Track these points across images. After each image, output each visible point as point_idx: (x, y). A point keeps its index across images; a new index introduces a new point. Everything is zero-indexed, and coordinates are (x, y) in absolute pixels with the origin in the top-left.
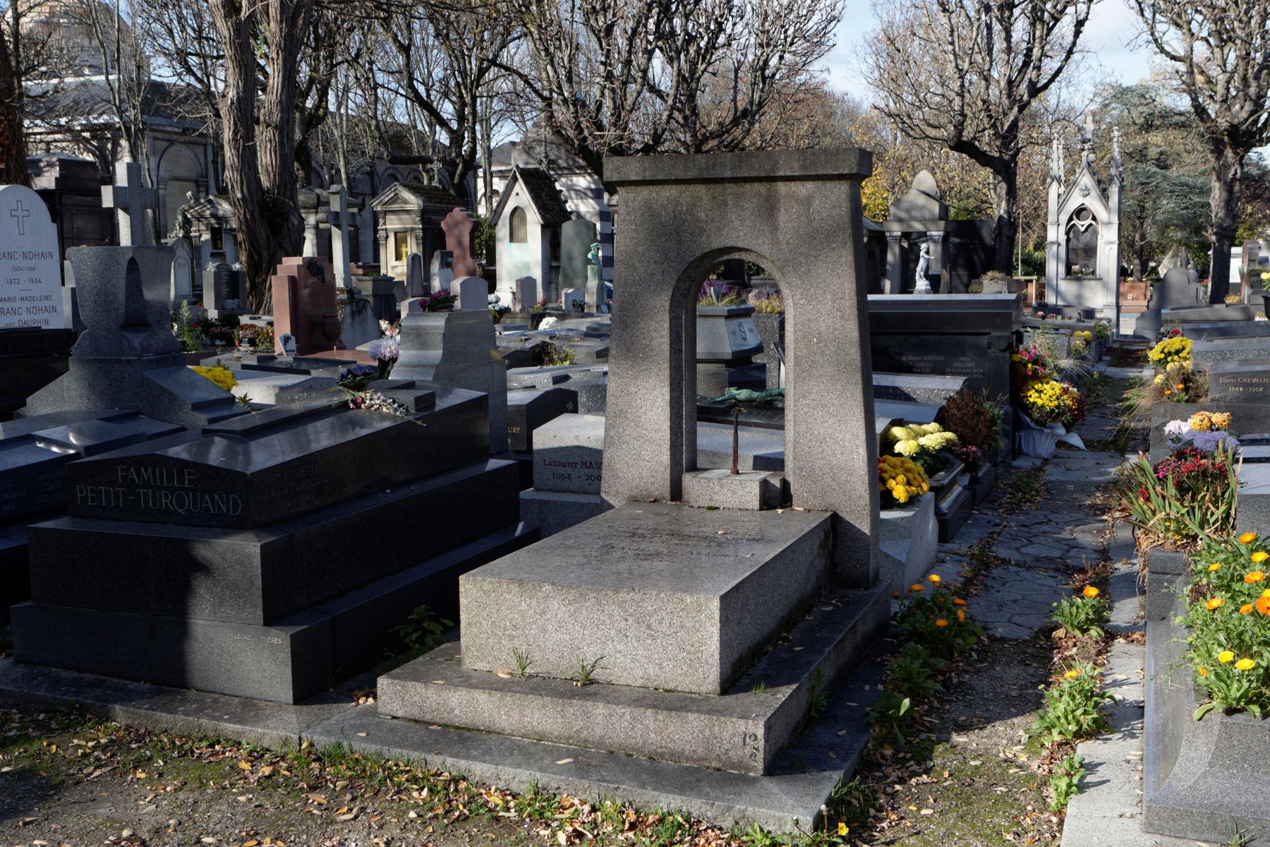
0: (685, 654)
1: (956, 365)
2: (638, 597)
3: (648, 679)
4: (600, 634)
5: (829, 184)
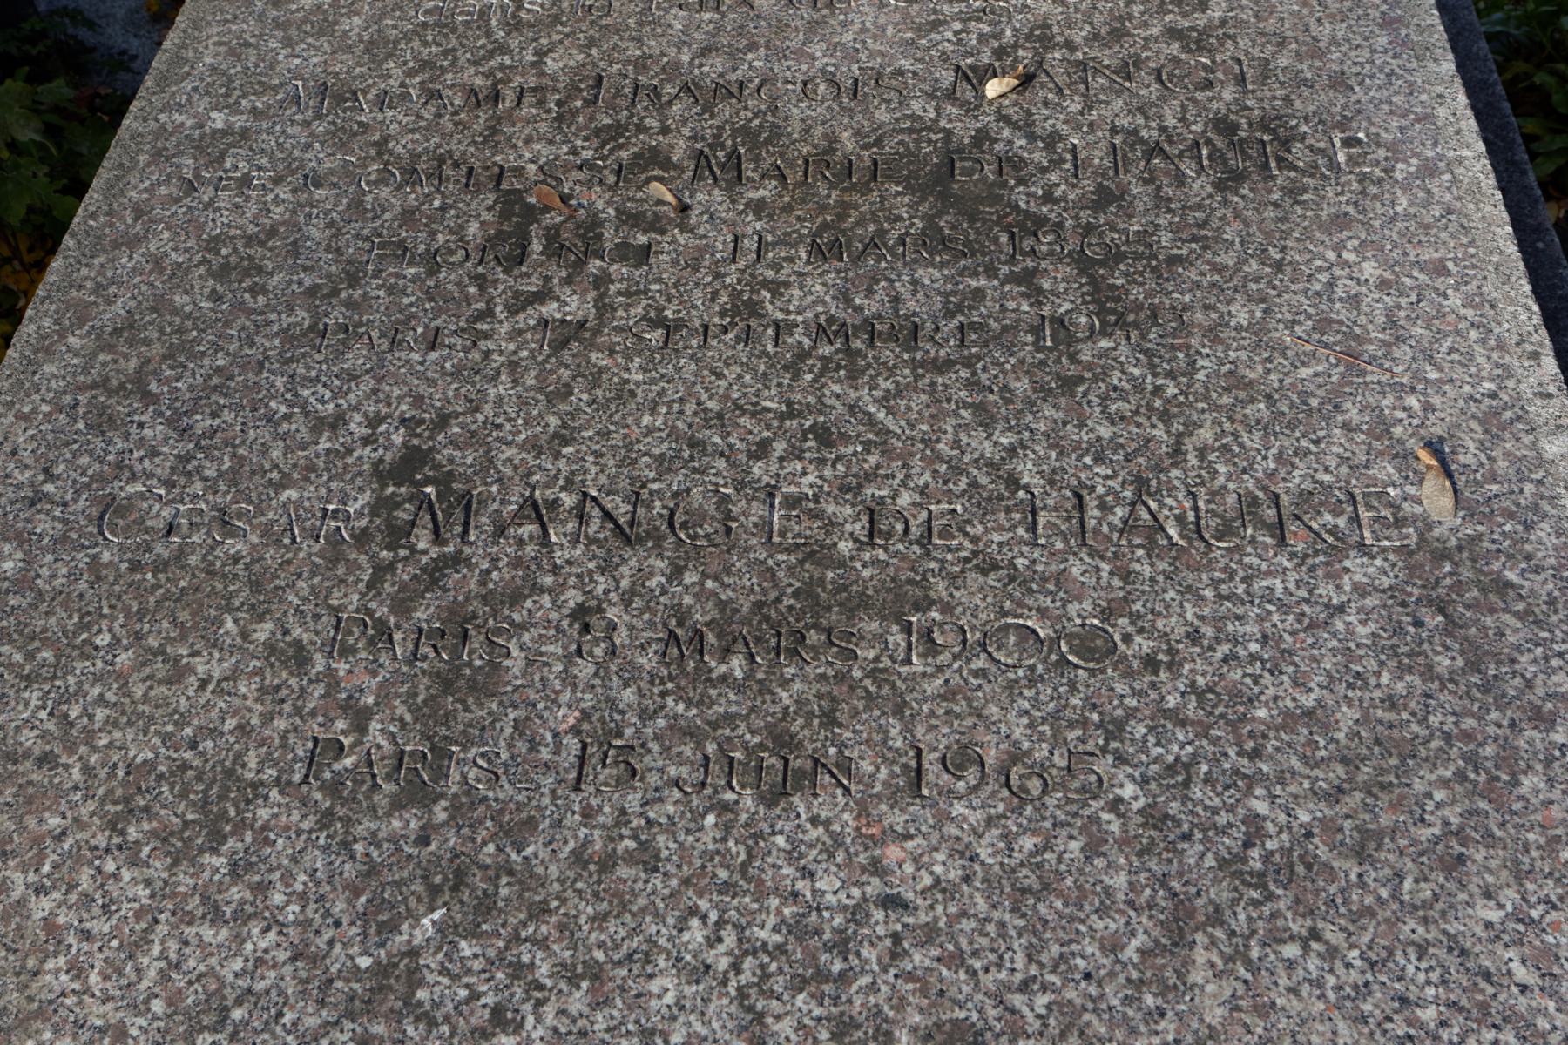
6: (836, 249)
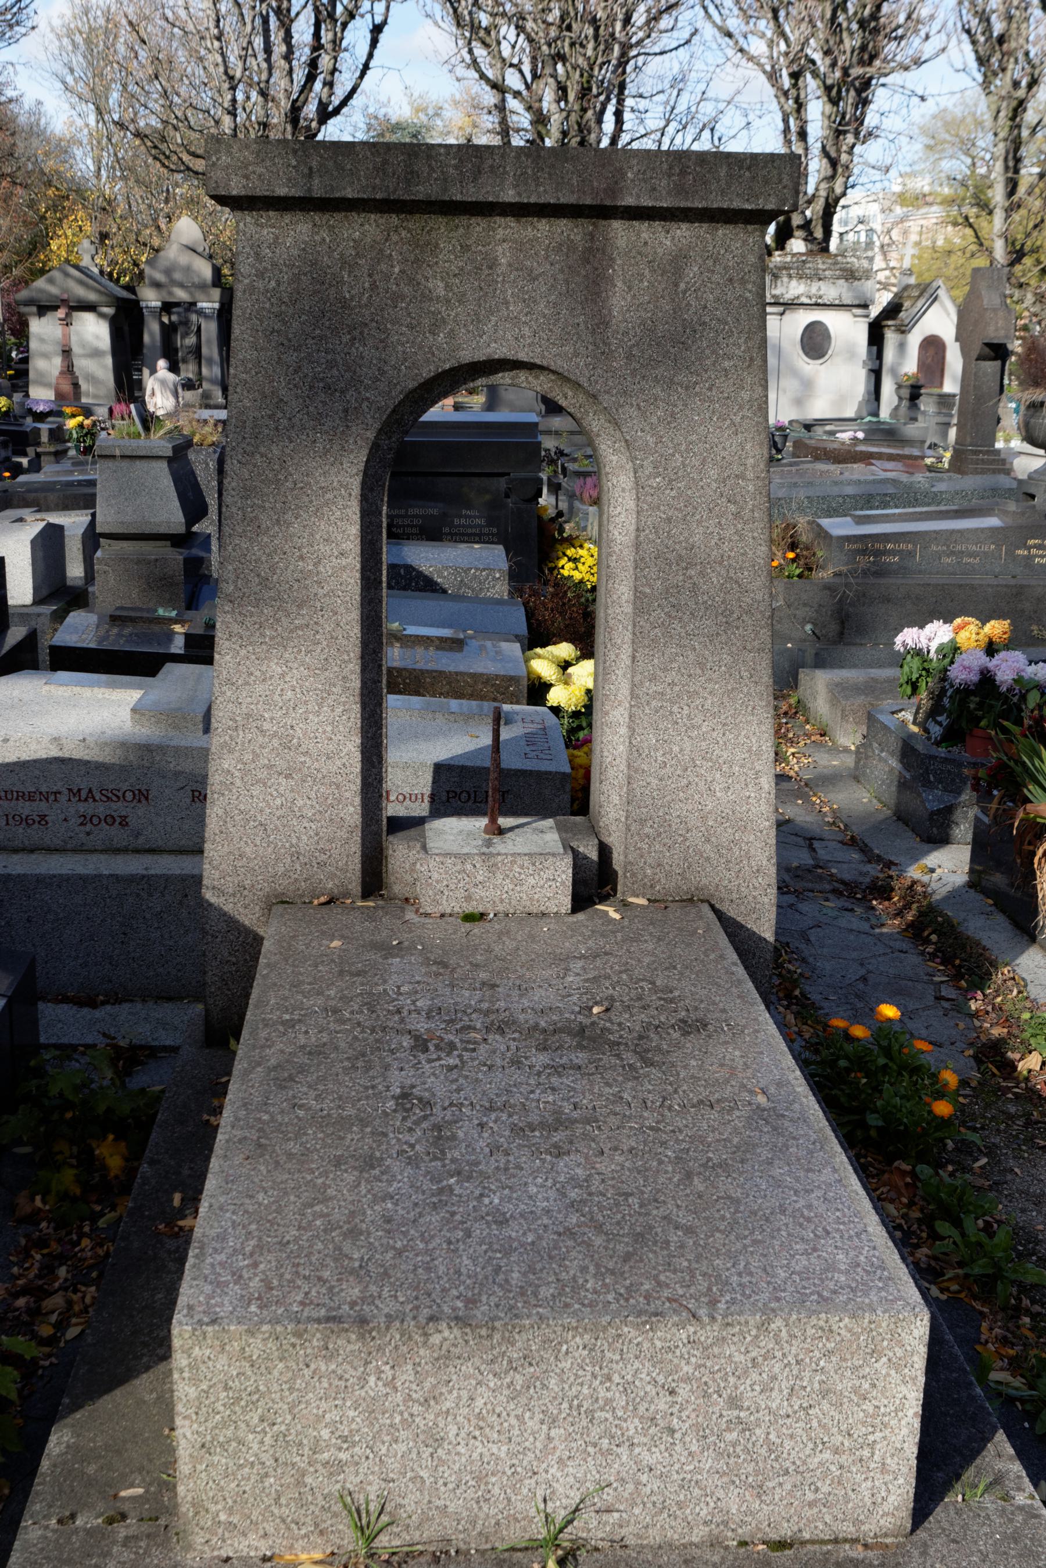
0: (827, 1455)
1: (456, 521)
2: (707, 1334)
3: (725, 1523)
4: (595, 1432)
5: (723, 231)
6: (545, 1049)
